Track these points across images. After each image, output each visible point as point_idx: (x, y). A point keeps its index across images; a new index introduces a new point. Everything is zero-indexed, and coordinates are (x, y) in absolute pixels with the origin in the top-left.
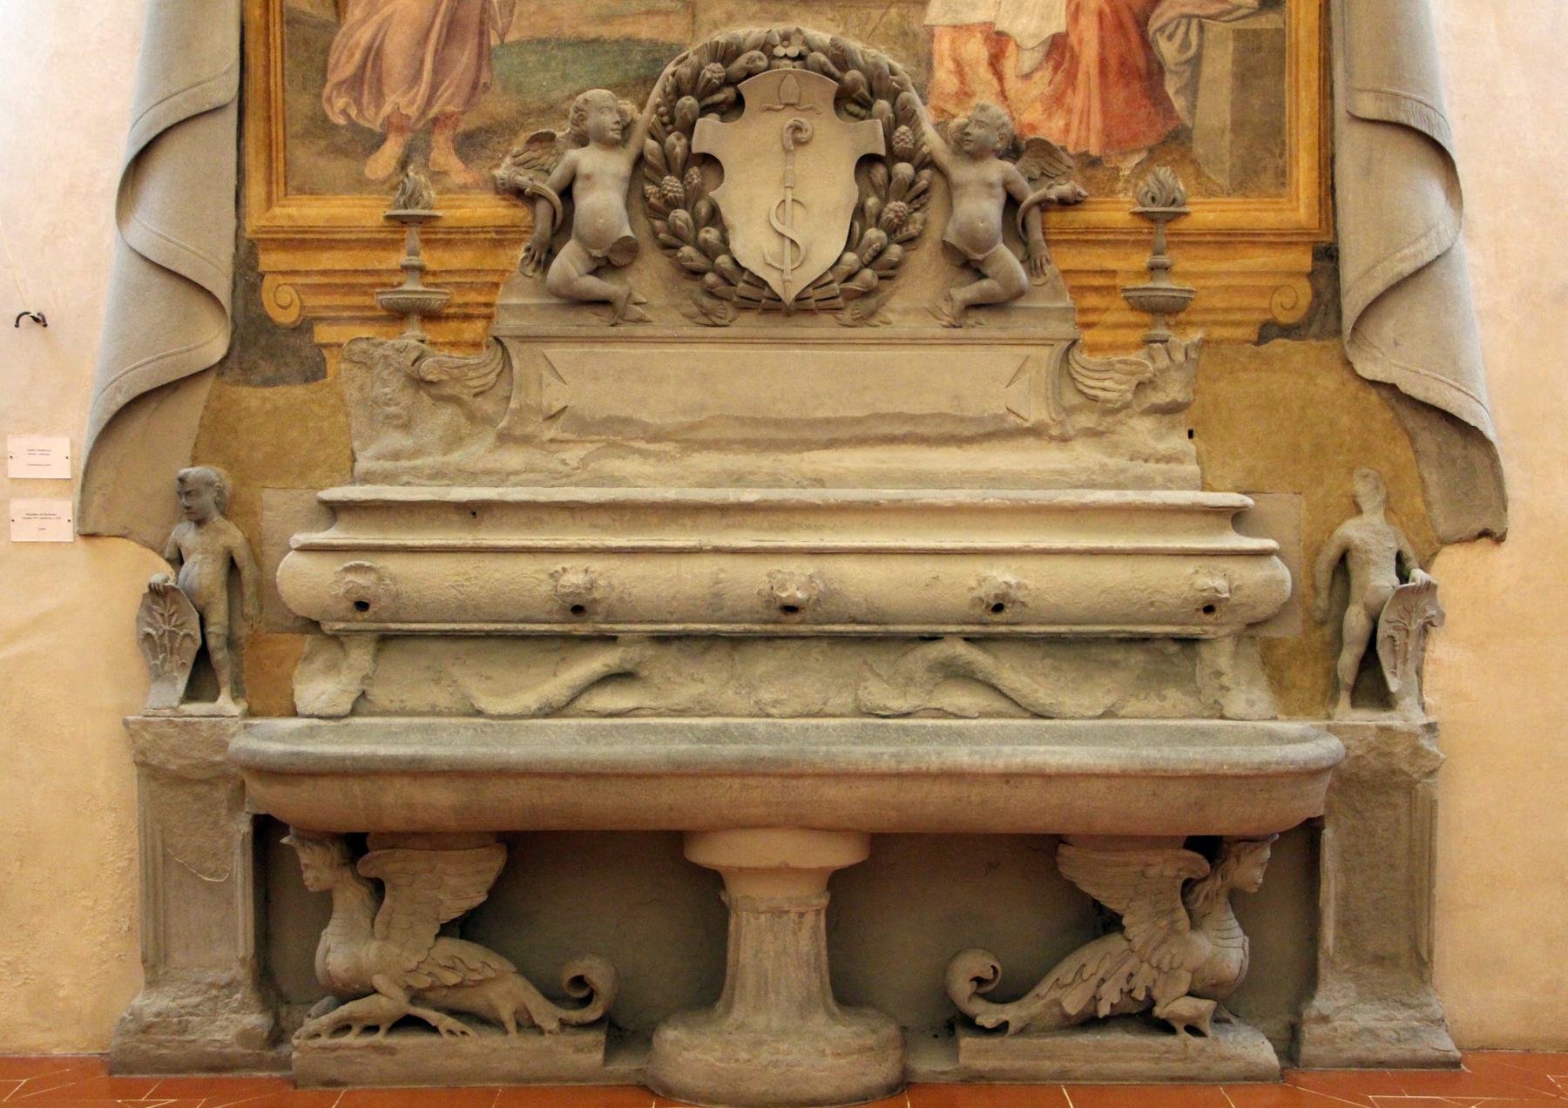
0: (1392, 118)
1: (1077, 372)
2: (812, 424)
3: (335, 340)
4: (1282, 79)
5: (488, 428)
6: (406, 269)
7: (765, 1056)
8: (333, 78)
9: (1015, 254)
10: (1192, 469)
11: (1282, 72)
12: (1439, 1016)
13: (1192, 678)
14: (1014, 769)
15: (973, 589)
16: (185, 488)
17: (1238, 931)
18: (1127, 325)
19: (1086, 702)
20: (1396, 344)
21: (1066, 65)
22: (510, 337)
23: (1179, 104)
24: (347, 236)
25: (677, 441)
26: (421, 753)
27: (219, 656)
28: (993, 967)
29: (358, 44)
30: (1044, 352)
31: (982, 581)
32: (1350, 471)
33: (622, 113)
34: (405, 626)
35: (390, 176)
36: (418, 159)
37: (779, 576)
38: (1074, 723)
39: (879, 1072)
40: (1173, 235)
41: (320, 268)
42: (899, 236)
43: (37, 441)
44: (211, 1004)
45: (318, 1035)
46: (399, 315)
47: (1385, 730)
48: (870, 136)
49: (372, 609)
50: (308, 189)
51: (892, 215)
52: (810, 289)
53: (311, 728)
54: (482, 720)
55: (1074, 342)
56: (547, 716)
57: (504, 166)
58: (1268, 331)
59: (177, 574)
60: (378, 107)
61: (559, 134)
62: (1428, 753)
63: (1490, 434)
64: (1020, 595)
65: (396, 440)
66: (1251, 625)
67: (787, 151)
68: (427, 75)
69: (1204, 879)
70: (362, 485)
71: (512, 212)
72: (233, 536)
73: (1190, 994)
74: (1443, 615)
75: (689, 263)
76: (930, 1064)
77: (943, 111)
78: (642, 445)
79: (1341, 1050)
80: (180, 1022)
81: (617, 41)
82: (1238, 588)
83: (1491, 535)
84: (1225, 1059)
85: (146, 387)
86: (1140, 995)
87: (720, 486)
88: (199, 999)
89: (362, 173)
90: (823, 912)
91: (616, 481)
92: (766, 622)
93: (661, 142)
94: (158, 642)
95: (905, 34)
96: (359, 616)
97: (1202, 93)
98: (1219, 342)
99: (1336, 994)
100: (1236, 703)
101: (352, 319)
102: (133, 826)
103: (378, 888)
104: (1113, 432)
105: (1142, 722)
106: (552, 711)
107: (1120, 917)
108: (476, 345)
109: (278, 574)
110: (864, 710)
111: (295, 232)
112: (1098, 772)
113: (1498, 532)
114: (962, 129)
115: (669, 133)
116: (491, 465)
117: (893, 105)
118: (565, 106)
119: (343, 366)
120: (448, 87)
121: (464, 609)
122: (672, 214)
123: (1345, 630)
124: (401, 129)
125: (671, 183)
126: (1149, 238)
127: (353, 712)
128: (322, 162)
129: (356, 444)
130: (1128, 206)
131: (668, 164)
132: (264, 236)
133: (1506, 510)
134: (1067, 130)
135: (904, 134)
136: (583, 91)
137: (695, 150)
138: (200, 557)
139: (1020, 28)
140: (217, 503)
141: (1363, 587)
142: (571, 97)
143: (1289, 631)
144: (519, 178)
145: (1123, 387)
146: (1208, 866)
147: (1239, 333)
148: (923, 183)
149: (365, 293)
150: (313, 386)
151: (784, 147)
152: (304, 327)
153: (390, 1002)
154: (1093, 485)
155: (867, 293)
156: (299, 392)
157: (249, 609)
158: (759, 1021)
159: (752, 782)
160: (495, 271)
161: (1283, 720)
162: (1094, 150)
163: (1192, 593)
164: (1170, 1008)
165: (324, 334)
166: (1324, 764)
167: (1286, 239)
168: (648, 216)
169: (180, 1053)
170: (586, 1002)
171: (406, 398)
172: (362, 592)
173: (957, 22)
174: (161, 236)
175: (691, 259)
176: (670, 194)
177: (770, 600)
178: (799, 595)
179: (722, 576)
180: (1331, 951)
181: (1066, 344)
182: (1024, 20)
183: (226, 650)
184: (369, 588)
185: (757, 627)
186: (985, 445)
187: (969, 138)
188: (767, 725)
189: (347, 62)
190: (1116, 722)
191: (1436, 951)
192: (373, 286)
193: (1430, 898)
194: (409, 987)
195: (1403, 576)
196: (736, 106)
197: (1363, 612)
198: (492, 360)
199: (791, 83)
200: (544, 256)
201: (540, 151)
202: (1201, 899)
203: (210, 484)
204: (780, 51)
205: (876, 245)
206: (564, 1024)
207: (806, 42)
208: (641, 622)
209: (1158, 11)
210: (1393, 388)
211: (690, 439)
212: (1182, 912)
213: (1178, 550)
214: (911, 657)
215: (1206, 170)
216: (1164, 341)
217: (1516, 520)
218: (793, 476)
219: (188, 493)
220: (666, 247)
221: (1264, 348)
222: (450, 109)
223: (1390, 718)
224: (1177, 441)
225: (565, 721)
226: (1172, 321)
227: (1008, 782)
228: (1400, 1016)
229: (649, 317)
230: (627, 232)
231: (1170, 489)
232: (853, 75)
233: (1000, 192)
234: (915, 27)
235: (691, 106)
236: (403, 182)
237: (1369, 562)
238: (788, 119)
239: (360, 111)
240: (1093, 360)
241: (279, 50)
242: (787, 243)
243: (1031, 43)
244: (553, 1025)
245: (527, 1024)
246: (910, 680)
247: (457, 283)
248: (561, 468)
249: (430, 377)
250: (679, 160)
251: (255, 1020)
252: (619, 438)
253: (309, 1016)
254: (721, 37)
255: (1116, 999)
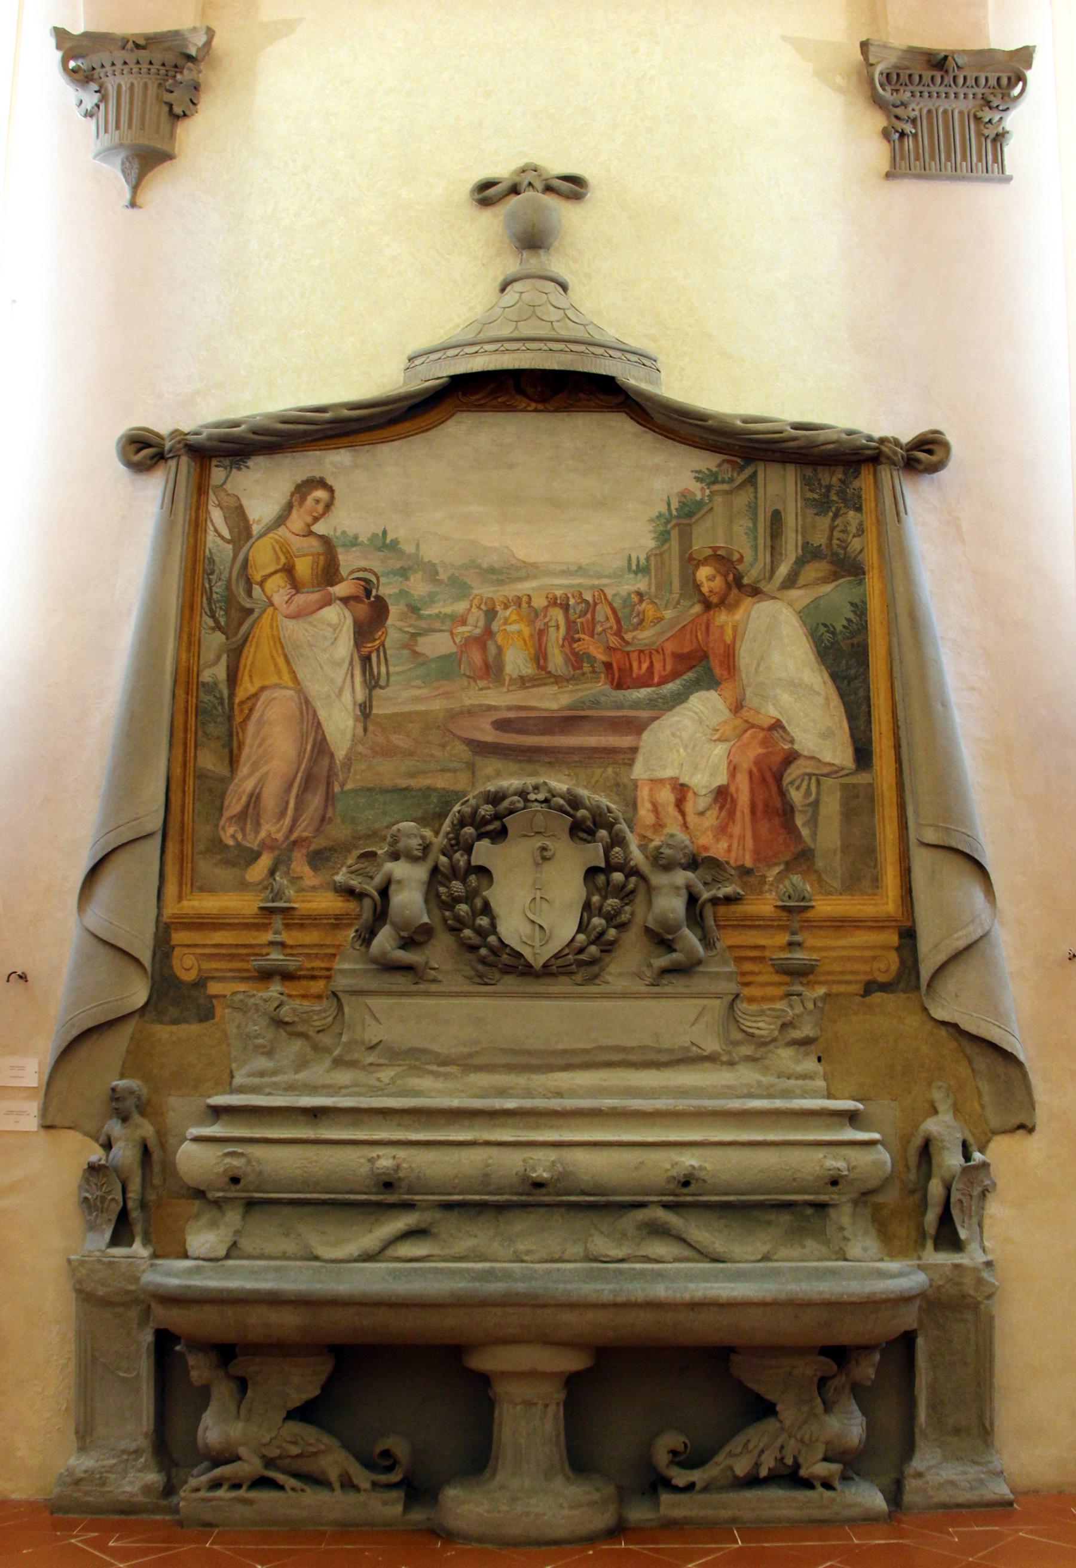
0: (947, 844)
1: (740, 1017)
2: (554, 1053)
3: (222, 993)
4: (873, 817)
5: (327, 1055)
6: (272, 944)
7: (519, 1508)
8: (227, 814)
9: (696, 936)
10: (820, 1083)
11: (873, 811)
12: (998, 1470)
13: (823, 1232)
14: (697, 1300)
15: (668, 1170)
16: (115, 1095)
17: (858, 1413)
18: (772, 984)
19: (750, 1249)
20: (957, 996)
21: (728, 806)
22: (345, 992)
23: (805, 832)
24: (232, 921)
25: (458, 1065)
26: (276, 1287)
27: (135, 1214)
28: (685, 1444)
29: (244, 792)
30: (717, 1003)
31: (675, 1164)
32: (929, 1084)
33: (423, 837)
34: (265, 1195)
35: (263, 880)
36: (283, 868)
37: (531, 1162)
38: (741, 1265)
39: (602, 1520)
40: (804, 921)
41: (214, 942)
42: (615, 922)
43: (16, 1061)
44: (122, 1466)
45: (197, 1490)
46: (266, 975)
47: (956, 1266)
48: (595, 854)
49: (242, 1183)
50: (207, 889)
51: (609, 908)
52: (553, 960)
53: (198, 1268)
54: (318, 1264)
55: (737, 996)
56: (365, 1261)
57: (341, 873)
58: (871, 987)
59: (107, 1156)
60: (257, 833)
61: (380, 852)
62: (988, 1282)
63: (1022, 1057)
64: (702, 1174)
65: (262, 1063)
66: (865, 1194)
67: (537, 864)
68: (290, 812)
69: (835, 1376)
70: (237, 1094)
71: (346, 905)
72: (146, 1129)
73: (825, 1459)
74: (994, 1184)
75: (469, 941)
76: (638, 1514)
77: (645, 837)
78: (434, 1068)
79: (931, 1497)
80: (101, 1478)
81: (420, 789)
82: (854, 1168)
83: (1027, 1128)
84: (850, 1506)
85: (90, 1024)
86: (789, 1461)
87: (489, 1097)
88: (114, 1461)
89: (243, 878)
90: (562, 1404)
91: (416, 1093)
92: (521, 1194)
93: (450, 858)
94: (92, 1204)
95: (618, 785)
96: (233, 1187)
97: (820, 825)
98: (837, 995)
99: (927, 1456)
100: (855, 1249)
101: (234, 978)
102: (71, 1335)
103: (243, 1384)
104: (765, 1058)
105: (788, 1264)
106: (369, 1257)
107: (774, 1405)
108: (319, 997)
109: (178, 1156)
110: (591, 1257)
111: (176, 918)
112: (756, 1301)
113: (1030, 1125)
114: (658, 848)
115: (456, 851)
116: (328, 1082)
117: (610, 833)
118: (384, 833)
119: (227, 1011)
120: (305, 820)
121: (307, 1184)
122: (457, 907)
123: (929, 1196)
124: (272, 848)
125: (457, 886)
126: (788, 923)
127: (228, 1256)
128: (217, 871)
129: (234, 1065)
130: (772, 901)
131: (454, 873)
132: (176, 921)
133: (1034, 1109)
134: (729, 850)
135: (617, 853)
136: (397, 822)
137: (473, 863)
138: (124, 1144)
139: (696, 781)
140: (137, 1106)
141: (940, 1166)
142: (388, 827)
143: (891, 1197)
144: (353, 882)
145: (772, 1027)
146: (835, 1367)
147: (851, 988)
148: (631, 886)
149: (243, 960)
150: (206, 1025)
151: (535, 861)
152: (200, 983)
153: (250, 1466)
154: (751, 1096)
155: (593, 962)
156: (193, 1029)
157: (157, 1181)
158: (515, 1483)
159: (511, 1310)
160: (333, 946)
161: (887, 1261)
162: (749, 864)
163: (822, 1171)
164: (810, 1470)
165: (214, 988)
166: (914, 1293)
167: (880, 924)
168: (440, 908)
169: (102, 1500)
170: (390, 1469)
171: (270, 1034)
172: (236, 1171)
173: (652, 777)
174: (106, 920)
175: (470, 938)
176: (456, 894)
177: (525, 1178)
178: (545, 1175)
179: (490, 1161)
180: (924, 1426)
181: (731, 997)
182: (699, 776)
183: (139, 1211)
184: (240, 1168)
185: (515, 1198)
186: (676, 1068)
187: (662, 856)
188: (522, 1268)
189: (236, 803)
190: (770, 1264)
191: (996, 1424)
192: (248, 955)
193: (991, 1386)
194: (264, 1456)
195: (967, 1157)
196: (500, 835)
197: (940, 1184)
198: (330, 1007)
199: (540, 817)
200: (367, 936)
201: (366, 863)
202: (832, 1390)
203: (132, 1092)
204: (532, 797)
205: (599, 929)
206: (375, 1485)
207: (550, 791)
208: (432, 1194)
209: (789, 771)
210: (955, 1026)
211: (467, 1064)
212: (819, 1401)
213: (811, 1141)
214: (624, 1219)
215: (824, 876)
216: (799, 995)
217: (1041, 1116)
218: (540, 1090)
219: (117, 1099)
220: (453, 930)
221: (868, 998)
222: (305, 834)
223: (961, 1258)
224: (810, 1065)
225: (379, 1265)
226: (805, 981)
227: (693, 1309)
228: (972, 1471)
229: (440, 978)
230: (426, 919)
231: (805, 1098)
232: (582, 813)
233: (684, 892)
234: (625, 780)
235: (471, 833)
236: (271, 883)
237: (943, 1148)
238: (538, 842)
239: (244, 836)
240: (750, 1007)
241: (191, 795)
242: (537, 927)
243: (703, 792)
244: (365, 1485)
245: (348, 1484)
246: (624, 1235)
247: (307, 954)
248: (377, 1084)
249: (287, 1019)
250: (462, 870)
251: (154, 1477)
252: (417, 1063)
253: (192, 1476)
254: (491, 787)
255: (772, 1464)
